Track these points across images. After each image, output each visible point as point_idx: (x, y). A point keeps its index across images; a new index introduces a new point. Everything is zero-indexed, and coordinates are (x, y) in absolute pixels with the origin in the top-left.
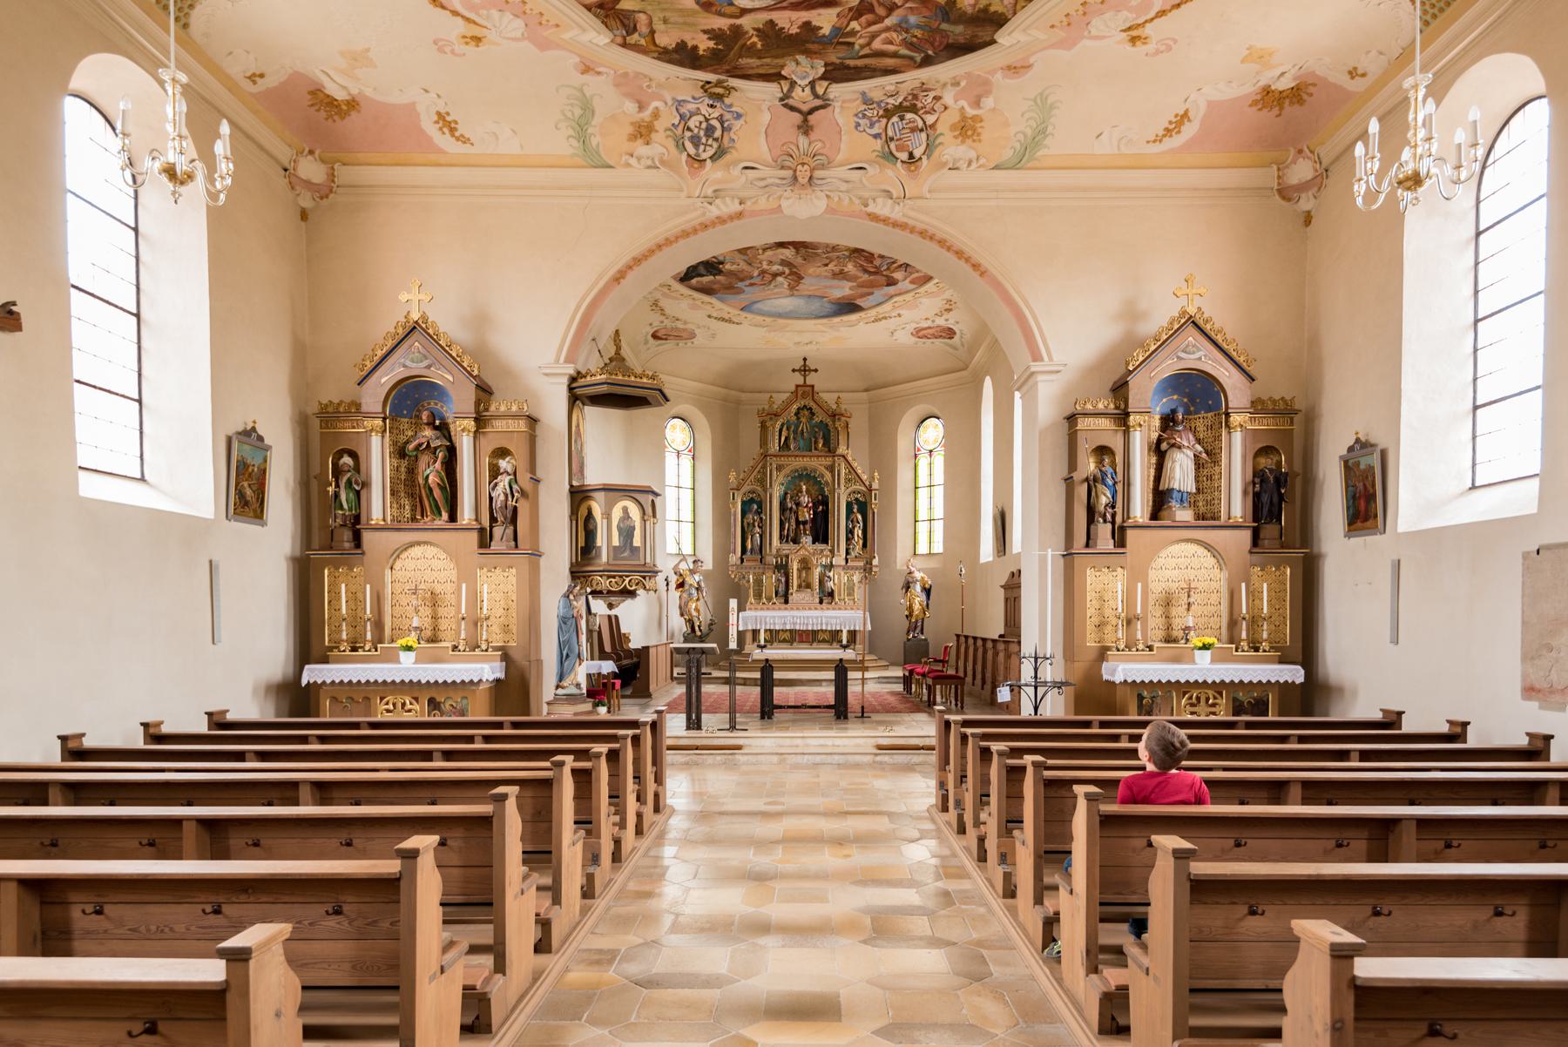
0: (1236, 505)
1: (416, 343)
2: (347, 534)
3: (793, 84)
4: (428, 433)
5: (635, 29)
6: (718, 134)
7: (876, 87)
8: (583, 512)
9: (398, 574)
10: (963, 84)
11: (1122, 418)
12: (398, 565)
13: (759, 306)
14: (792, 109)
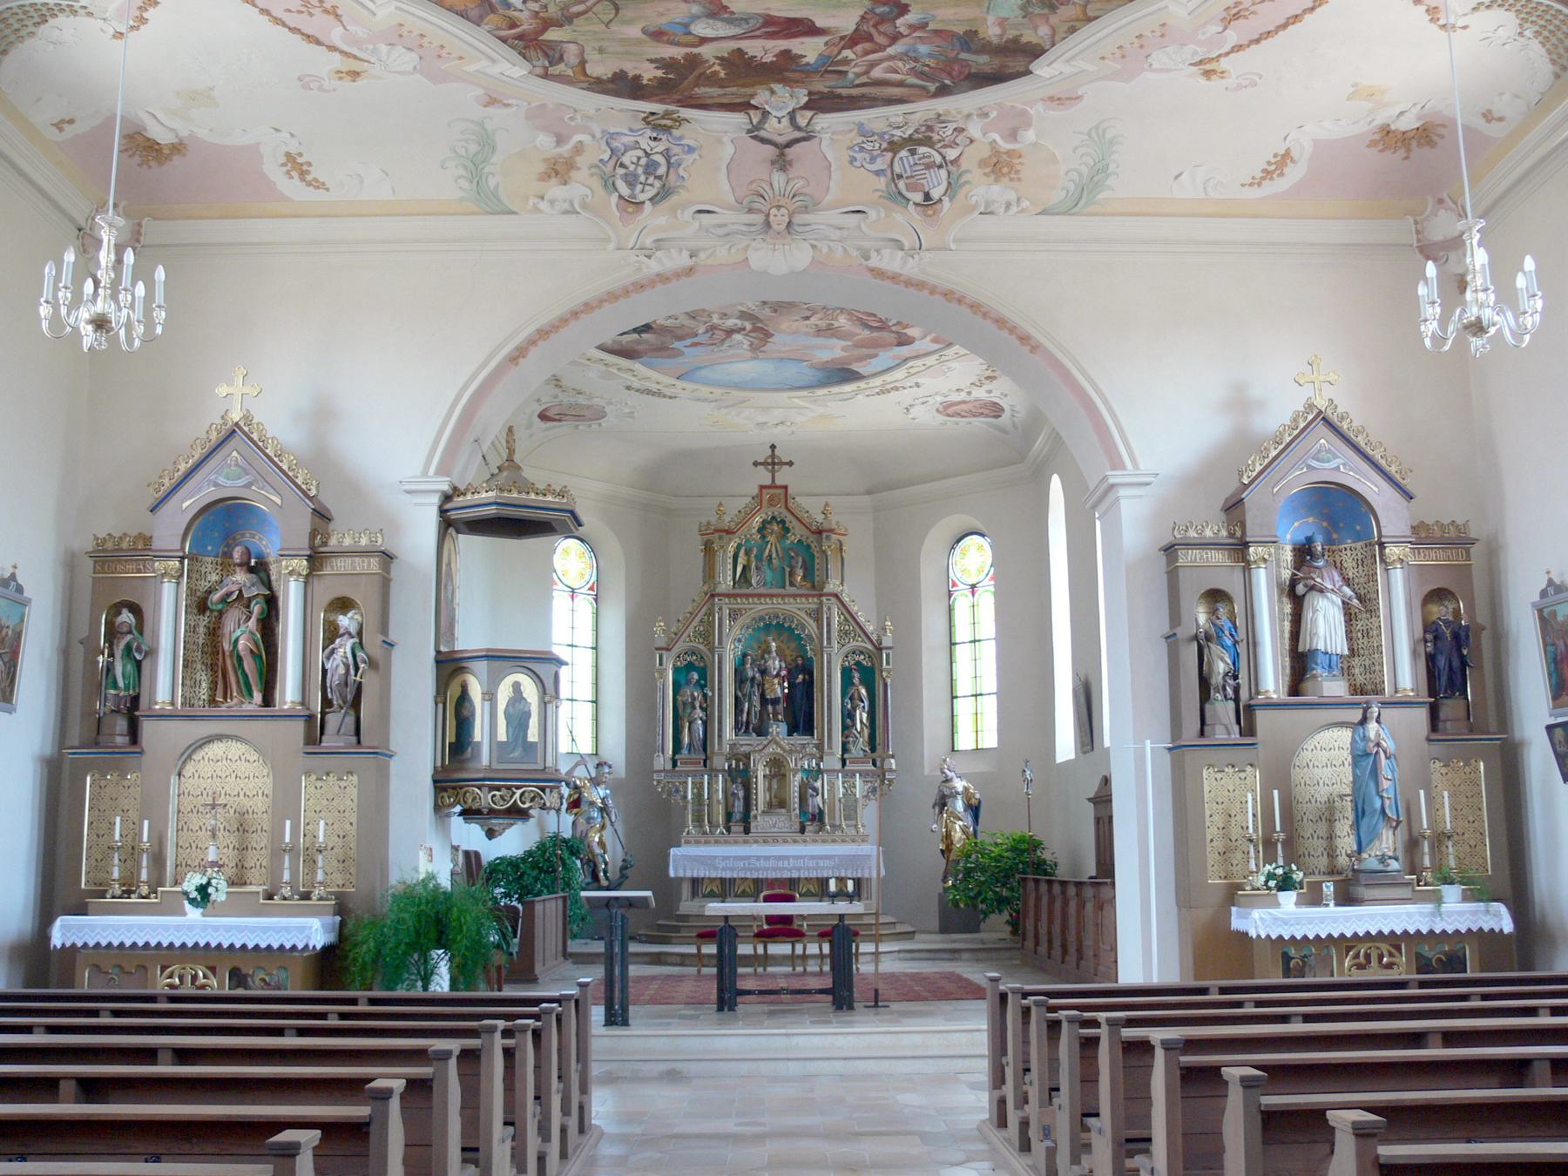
0: (1403, 670)
1: (233, 454)
2: (122, 724)
3: (766, 114)
4: (241, 577)
5: (561, 59)
6: (662, 170)
7: (876, 118)
8: (453, 692)
9: (189, 784)
10: (993, 114)
11: (1239, 549)
12: (189, 770)
13: (703, 373)
14: (764, 141)
